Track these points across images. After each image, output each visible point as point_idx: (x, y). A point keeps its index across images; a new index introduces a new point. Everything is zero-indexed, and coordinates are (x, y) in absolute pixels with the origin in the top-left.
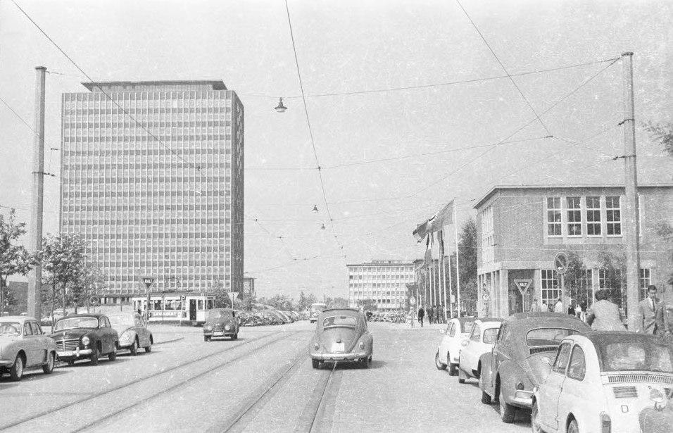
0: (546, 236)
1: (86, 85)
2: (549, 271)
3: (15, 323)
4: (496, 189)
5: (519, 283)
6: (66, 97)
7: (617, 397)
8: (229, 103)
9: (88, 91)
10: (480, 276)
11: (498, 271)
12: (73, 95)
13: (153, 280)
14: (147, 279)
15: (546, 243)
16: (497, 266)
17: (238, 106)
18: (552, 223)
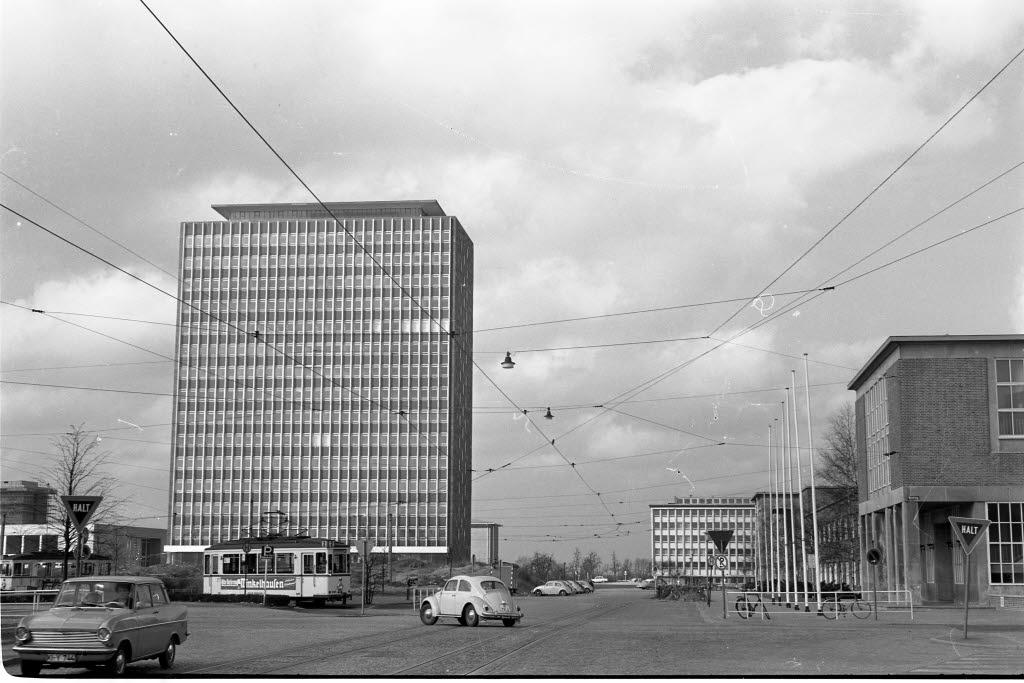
0: (997, 436)
1: (218, 209)
2: (1004, 507)
3: (316, 603)
4: (892, 343)
5: (960, 525)
6: (188, 228)
7: (182, 223)
8: (443, 236)
9: (224, 220)
10: (863, 517)
11: (899, 506)
12: (197, 226)
13: (92, 503)
14: (78, 503)
15: (996, 448)
16: (897, 496)
17: (463, 246)
18: (819, 597)
